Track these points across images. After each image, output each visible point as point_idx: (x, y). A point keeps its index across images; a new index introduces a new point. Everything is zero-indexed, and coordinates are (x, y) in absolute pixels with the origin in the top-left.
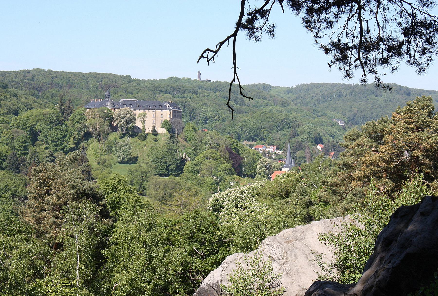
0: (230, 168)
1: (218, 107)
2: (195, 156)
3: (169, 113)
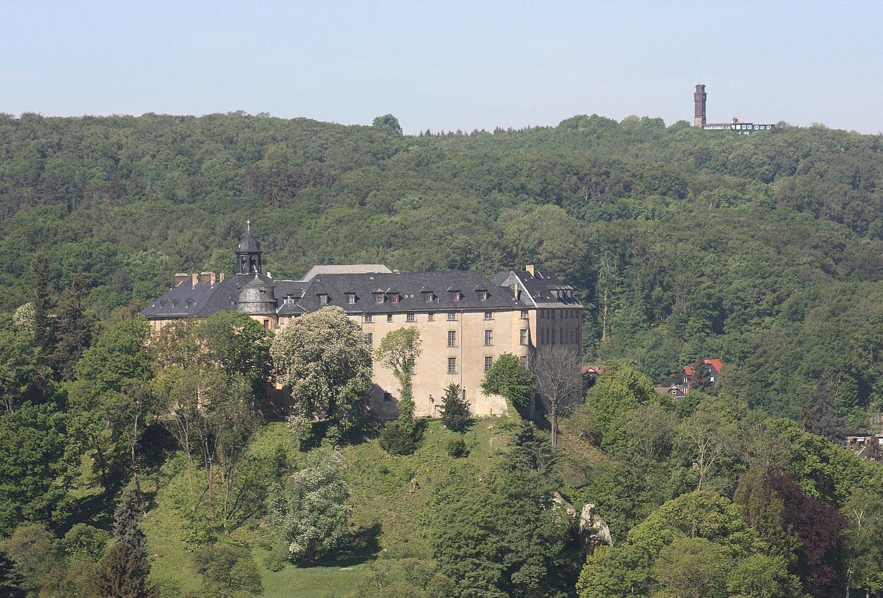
0: (783, 573)
1: (772, 253)
2: (630, 523)
3: (522, 324)
